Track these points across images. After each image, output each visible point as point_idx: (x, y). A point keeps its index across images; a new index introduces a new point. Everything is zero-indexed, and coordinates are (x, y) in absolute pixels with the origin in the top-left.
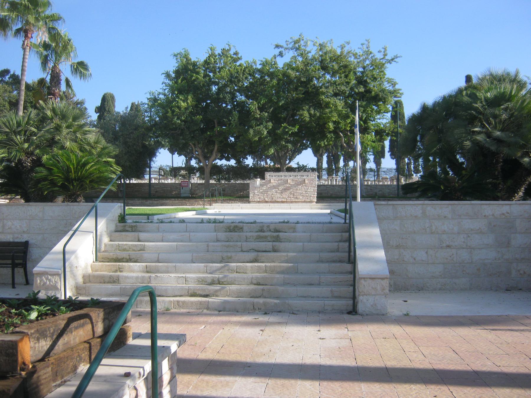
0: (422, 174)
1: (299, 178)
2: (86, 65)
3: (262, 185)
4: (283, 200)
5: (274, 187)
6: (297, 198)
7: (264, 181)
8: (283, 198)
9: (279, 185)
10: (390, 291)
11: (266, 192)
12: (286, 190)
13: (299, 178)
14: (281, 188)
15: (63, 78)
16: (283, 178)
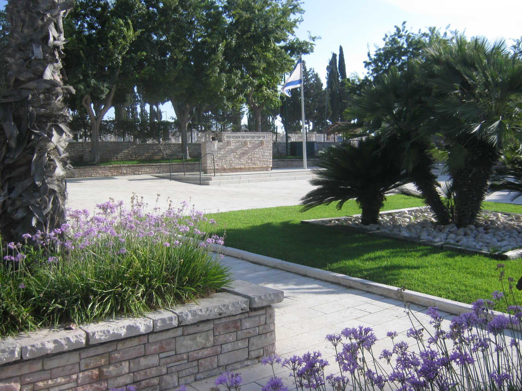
0: (494, 167)
1: (256, 139)
2: (333, 62)
3: (219, 149)
4: (243, 166)
5: (232, 151)
6: (254, 164)
7: (221, 144)
8: (241, 164)
9: (237, 148)
10: (283, 292)
11: (224, 157)
12: (244, 154)
13: (256, 139)
14: (239, 152)
15: (462, 72)
16: (240, 139)
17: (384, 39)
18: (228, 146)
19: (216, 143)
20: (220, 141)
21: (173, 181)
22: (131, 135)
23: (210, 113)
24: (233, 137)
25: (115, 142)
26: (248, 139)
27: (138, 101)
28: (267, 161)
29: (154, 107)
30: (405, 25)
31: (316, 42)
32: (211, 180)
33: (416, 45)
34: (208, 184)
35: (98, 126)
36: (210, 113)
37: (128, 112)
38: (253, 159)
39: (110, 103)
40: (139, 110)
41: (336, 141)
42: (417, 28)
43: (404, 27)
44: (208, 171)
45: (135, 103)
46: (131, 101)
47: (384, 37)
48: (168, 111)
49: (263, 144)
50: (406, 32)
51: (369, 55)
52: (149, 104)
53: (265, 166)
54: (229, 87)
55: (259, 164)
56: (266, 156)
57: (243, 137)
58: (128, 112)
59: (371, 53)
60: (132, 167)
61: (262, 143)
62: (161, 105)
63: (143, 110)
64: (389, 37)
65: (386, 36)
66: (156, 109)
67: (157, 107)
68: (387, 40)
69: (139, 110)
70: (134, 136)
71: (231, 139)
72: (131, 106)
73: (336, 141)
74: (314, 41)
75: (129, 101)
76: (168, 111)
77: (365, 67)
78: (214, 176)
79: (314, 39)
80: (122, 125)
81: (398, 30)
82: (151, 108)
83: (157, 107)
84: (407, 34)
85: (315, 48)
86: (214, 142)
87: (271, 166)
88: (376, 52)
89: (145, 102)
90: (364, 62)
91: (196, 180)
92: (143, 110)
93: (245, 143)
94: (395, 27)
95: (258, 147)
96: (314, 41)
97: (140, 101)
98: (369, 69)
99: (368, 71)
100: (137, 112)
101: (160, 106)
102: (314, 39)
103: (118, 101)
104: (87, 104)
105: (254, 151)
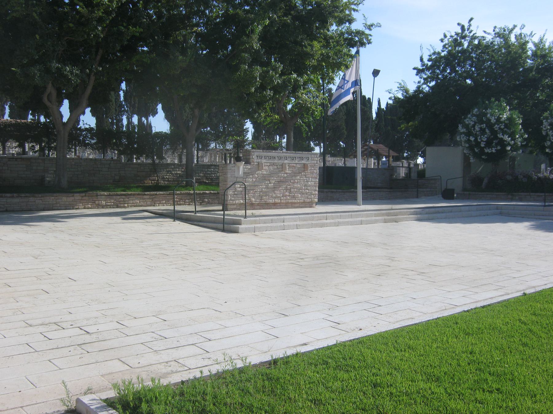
4: (277, 201)
5: (265, 178)
6: (294, 197)
8: (275, 198)
9: (271, 174)
13: (297, 162)
16: (276, 161)
17: (442, 40)
18: (259, 170)
19: (242, 167)
20: (247, 162)
21: (177, 222)
22: (114, 150)
23: (209, 129)
24: (265, 157)
25: (95, 160)
26: (286, 161)
27: (125, 111)
28: (311, 194)
29: (143, 119)
30: (471, 22)
31: (374, 32)
32: (240, 224)
33: (483, 48)
34: (236, 231)
35: (67, 135)
36: (209, 129)
37: (112, 123)
38: (292, 190)
39: (85, 102)
40: (125, 122)
41: (380, 167)
42: (484, 29)
43: (470, 25)
44: (229, 207)
45: (120, 113)
46: (116, 110)
47: (442, 37)
48: (160, 123)
49: (307, 169)
50: (470, 32)
51: (421, 60)
52: (138, 115)
53: (309, 200)
54: (263, 87)
55: (300, 198)
56: (310, 186)
57: (280, 158)
58: (112, 123)
59: (424, 57)
60: (115, 197)
61: (305, 167)
62: (151, 117)
63: (130, 122)
64: (448, 37)
65: (445, 36)
66: (145, 122)
67: (147, 119)
68: (446, 41)
69: (125, 122)
70: (119, 151)
71: (264, 161)
72: (115, 117)
73: (380, 167)
74: (370, 30)
75: (114, 111)
76: (160, 123)
77: (417, 75)
78: (245, 217)
79: (370, 27)
80: (104, 136)
81: (463, 28)
82: (140, 120)
83: (147, 119)
84: (471, 34)
85: (373, 39)
86: (238, 163)
87: (316, 200)
88: (430, 56)
89: (133, 113)
90: (414, 69)
91: (214, 222)
92: (130, 122)
93: (283, 166)
94: (459, 24)
95: (300, 173)
96: (370, 30)
97: (127, 112)
98: (421, 78)
99: (420, 80)
100: (122, 125)
101: (151, 118)
102: (370, 27)
103: (101, 103)
104: (51, 102)
105: (294, 178)
